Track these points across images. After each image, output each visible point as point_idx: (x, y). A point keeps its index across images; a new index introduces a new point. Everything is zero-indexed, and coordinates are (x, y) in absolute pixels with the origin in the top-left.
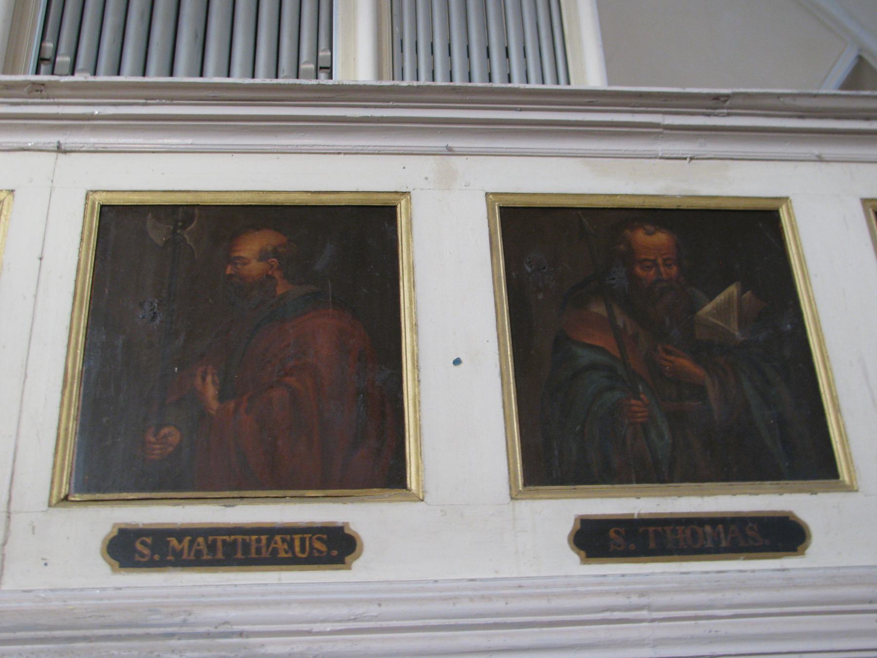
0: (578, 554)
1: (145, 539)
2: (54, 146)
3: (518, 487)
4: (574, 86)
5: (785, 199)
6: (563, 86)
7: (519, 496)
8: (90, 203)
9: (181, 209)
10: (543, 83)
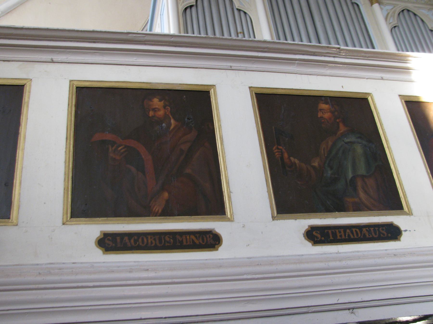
0: (101, 249)
1: (109, 237)
2: (380, 78)
3: (67, 217)
4: (257, 38)
5: (213, 86)
6: (252, 38)
7: (67, 223)
8: (71, 85)
9: (323, 98)
10: (193, 34)
